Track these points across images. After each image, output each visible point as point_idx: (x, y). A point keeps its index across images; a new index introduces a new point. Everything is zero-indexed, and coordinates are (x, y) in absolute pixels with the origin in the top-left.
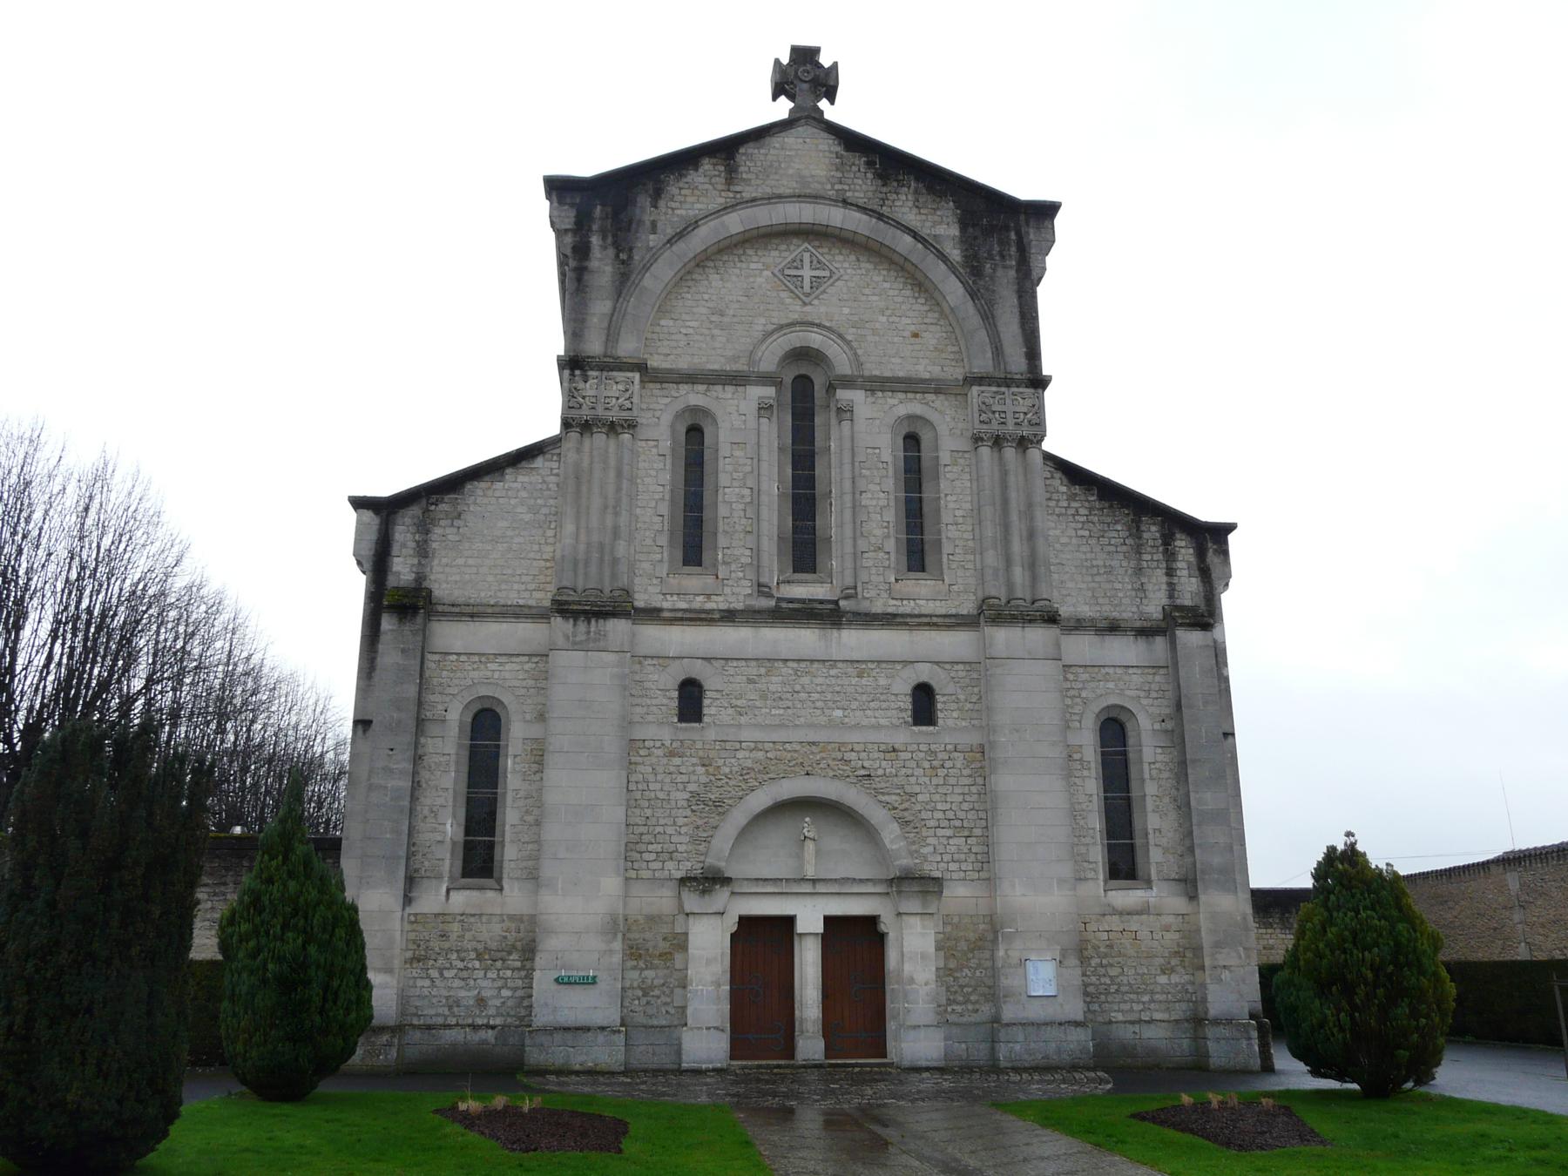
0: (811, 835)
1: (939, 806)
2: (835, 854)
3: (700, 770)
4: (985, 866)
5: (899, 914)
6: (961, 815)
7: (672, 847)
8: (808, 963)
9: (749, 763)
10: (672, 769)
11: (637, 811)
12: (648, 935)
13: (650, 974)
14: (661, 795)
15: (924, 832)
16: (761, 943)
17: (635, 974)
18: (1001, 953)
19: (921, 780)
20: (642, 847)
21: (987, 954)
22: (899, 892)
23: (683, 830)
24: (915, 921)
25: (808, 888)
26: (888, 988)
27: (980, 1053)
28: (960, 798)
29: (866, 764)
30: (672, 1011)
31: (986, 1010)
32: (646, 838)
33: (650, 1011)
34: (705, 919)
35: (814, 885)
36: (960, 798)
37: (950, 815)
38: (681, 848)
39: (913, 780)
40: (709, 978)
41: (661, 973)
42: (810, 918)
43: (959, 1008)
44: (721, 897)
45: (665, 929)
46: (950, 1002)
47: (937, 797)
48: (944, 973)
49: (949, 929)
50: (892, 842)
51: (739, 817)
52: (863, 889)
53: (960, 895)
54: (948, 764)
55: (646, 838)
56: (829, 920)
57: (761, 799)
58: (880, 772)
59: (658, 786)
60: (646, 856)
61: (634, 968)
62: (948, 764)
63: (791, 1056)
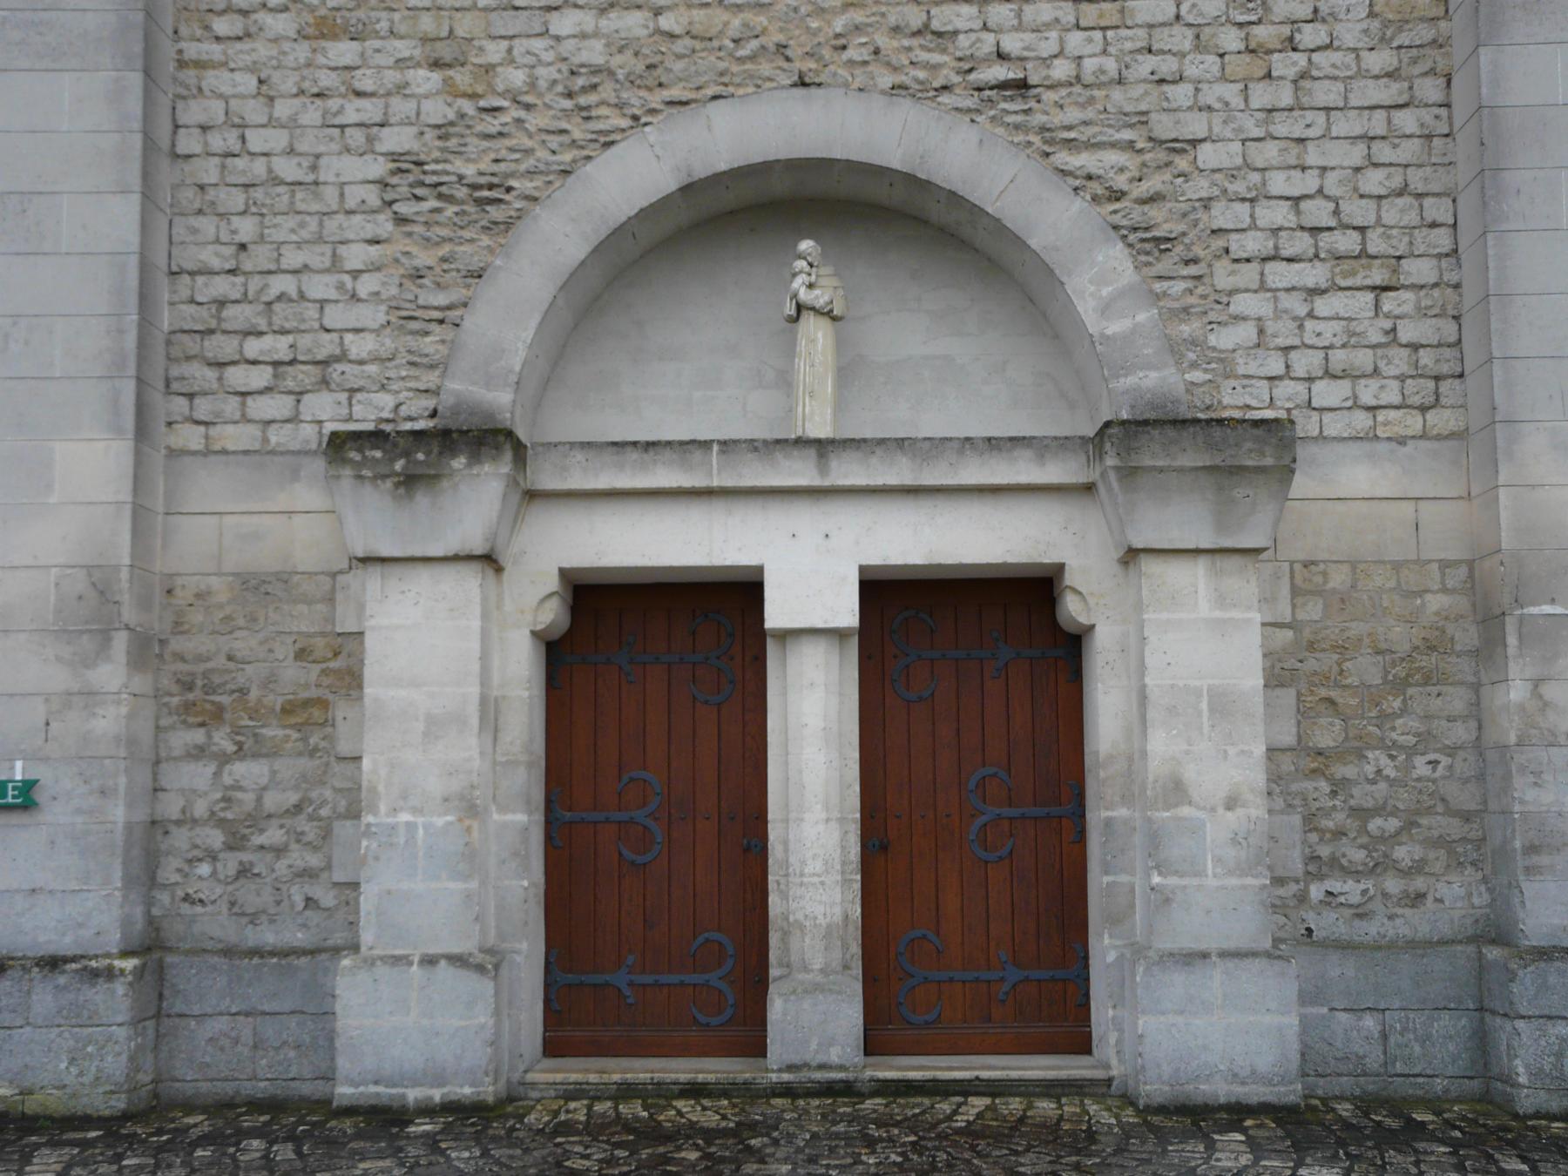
0: (819, 297)
1: (1279, 183)
2: (933, 364)
3: (425, 80)
4: (1454, 389)
5: (1131, 556)
6: (1359, 212)
7: (327, 346)
8: (812, 729)
9: (594, 53)
10: (327, 80)
11: (208, 225)
12: (244, 644)
13: (249, 772)
14: (288, 169)
15: (1223, 276)
16: (648, 666)
17: (198, 775)
18: (1517, 692)
19: (1210, 95)
20: (223, 346)
21: (1457, 700)
22: (1129, 474)
23: (366, 285)
24: (1192, 577)
25: (799, 471)
26: (1096, 816)
27: (1434, 1052)
28: (1356, 155)
29: (1011, 44)
30: (327, 898)
31: (1455, 898)
32: (237, 315)
33: (253, 896)
34: (422, 581)
35: (820, 464)
36: (1356, 155)
37: (1318, 212)
38: (359, 346)
39: (1181, 94)
40: (435, 785)
41: (289, 768)
42: (811, 576)
43: (1351, 890)
44: (474, 500)
45: (304, 620)
46: (1317, 867)
47: (1269, 153)
48: (1297, 768)
49: (1312, 610)
50: (1105, 309)
51: (559, 236)
52: (1024, 471)
53: (1358, 491)
54: (1310, 35)
55: (237, 315)
56: (881, 591)
57: (638, 173)
58: (1061, 70)
59: (276, 140)
60: (238, 377)
61: (198, 753)
62: (1310, 35)
63: (756, 1047)
